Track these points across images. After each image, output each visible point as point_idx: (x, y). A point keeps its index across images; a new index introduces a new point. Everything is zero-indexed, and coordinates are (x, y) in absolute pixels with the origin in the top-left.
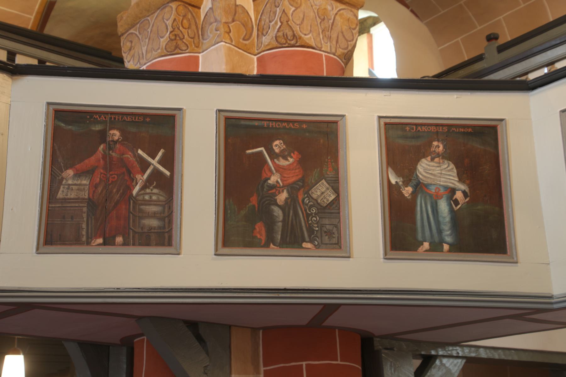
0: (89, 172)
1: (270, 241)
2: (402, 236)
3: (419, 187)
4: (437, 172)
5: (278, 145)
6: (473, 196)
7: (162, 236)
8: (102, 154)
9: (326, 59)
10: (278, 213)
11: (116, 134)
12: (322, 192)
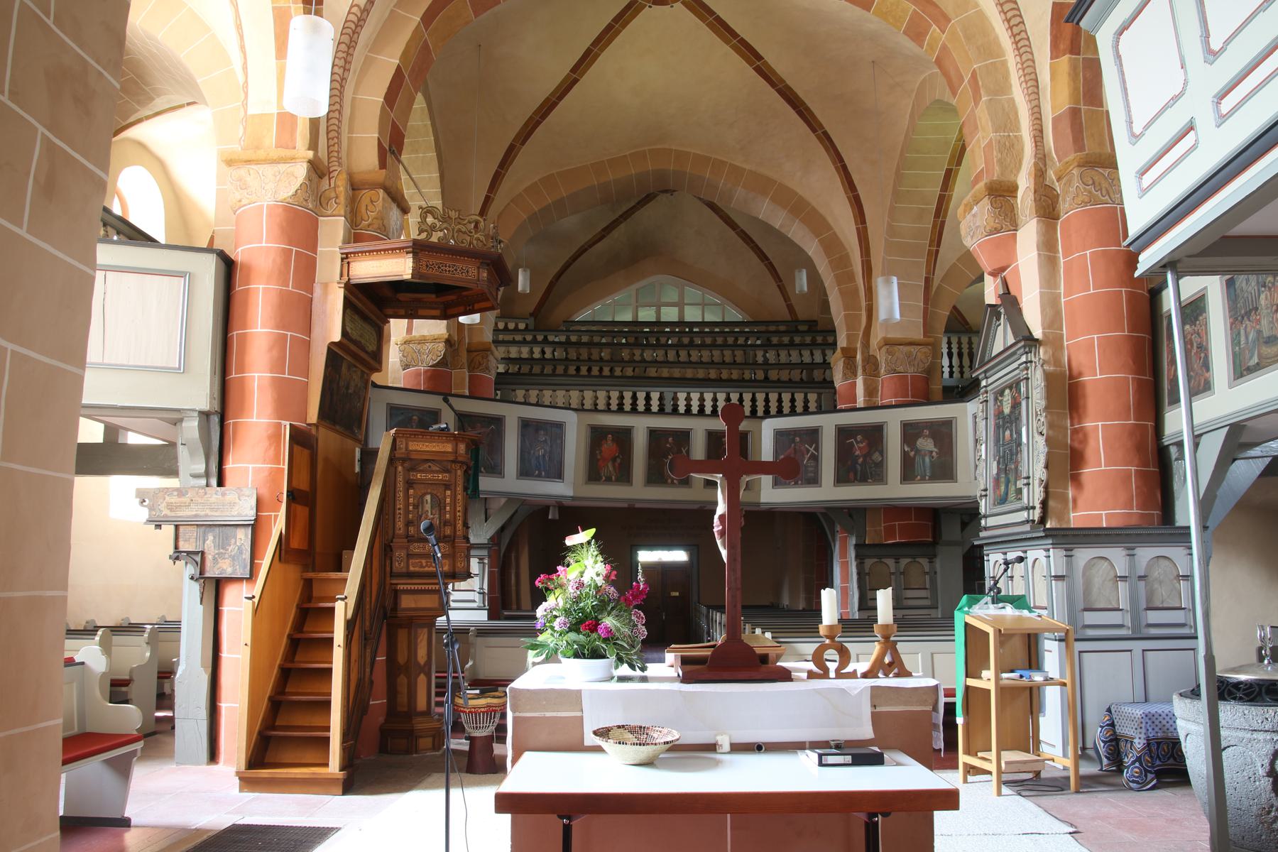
1: (856, 479)
3: (918, 451)
4: (926, 444)
5: (859, 438)
10: (859, 468)
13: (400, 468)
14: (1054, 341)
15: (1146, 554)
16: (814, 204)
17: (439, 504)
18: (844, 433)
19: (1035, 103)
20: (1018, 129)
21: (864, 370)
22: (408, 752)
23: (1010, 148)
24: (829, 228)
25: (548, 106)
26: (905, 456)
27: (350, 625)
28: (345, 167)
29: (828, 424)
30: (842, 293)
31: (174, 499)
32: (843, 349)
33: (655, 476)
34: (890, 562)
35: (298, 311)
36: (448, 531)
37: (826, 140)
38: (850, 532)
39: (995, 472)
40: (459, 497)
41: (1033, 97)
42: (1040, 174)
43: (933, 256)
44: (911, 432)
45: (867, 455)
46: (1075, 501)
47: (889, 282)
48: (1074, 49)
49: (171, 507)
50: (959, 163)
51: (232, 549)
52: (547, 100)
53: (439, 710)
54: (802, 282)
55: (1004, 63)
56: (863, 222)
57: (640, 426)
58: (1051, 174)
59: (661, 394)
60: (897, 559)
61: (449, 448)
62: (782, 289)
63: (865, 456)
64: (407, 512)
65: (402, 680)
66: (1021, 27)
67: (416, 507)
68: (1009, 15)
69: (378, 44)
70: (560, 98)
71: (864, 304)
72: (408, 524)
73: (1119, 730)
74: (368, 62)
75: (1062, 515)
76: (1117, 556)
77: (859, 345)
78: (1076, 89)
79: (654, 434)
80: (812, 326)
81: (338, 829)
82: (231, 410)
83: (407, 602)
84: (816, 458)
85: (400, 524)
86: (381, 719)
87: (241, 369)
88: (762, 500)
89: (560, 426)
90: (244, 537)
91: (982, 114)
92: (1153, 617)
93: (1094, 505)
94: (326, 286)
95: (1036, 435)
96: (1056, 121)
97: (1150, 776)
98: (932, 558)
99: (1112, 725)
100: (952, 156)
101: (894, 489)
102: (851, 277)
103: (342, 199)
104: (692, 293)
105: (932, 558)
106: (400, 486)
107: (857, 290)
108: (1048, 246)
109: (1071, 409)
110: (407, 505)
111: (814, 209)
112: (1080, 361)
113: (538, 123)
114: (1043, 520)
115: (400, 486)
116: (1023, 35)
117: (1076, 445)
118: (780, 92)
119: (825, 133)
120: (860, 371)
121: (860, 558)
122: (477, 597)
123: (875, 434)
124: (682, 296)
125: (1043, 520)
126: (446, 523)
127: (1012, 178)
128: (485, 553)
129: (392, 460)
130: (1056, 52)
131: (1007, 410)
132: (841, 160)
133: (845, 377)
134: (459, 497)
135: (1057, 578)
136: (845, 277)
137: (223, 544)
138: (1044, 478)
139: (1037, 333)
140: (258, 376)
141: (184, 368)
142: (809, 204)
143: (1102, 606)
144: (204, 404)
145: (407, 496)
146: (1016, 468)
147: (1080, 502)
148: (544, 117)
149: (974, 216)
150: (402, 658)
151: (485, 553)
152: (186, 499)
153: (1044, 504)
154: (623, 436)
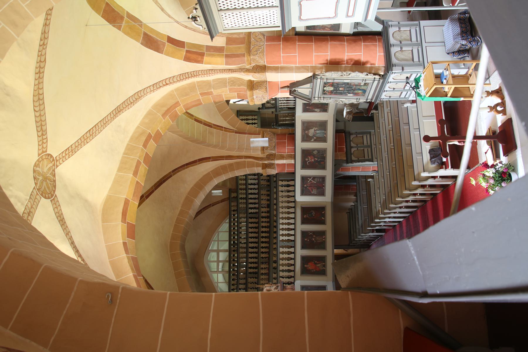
0: (312, 190)
1: (324, 161)
2: (324, 140)
3: (314, 135)
4: (311, 132)
5: (307, 160)
6: (316, 127)
7: (323, 179)
8: (320, 130)
9: (394, 9)
11: (305, 186)
12: (315, 152)
14: (313, 69)
15: (392, 41)
16: (197, 180)
18: (304, 166)
19: (218, 71)
20: (226, 79)
21: (273, 160)
23: (233, 82)
24: (208, 174)
26: (315, 141)
29: (300, 173)
30: (238, 169)
32: (262, 169)
33: (322, 246)
34: (353, 150)
37: (175, 171)
39: (352, 95)
41: (216, 72)
42: (248, 71)
43: (226, 129)
44: (306, 138)
45: (314, 156)
46: (371, 64)
47: (253, 142)
48: (202, 55)
50: (192, 115)
54: (218, 192)
55: (198, 82)
56: (209, 158)
58: (248, 67)
59: (281, 247)
60: (351, 147)
62: (218, 203)
63: (315, 157)
66: (189, 73)
68: (184, 77)
71: (243, 160)
73: (456, 50)
75: (378, 69)
76: (393, 50)
77: (261, 162)
78: (218, 55)
79: (303, 247)
80: (230, 191)
84: (314, 178)
88: (330, 201)
91: (215, 92)
92: (414, 39)
93: (374, 56)
95: (350, 76)
96: (227, 64)
97: (476, 39)
98: (350, 134)
99: (453, 52)
100: (190, 118)
101: (329, 145)
102: (231, 165)
104: (213, 246)
105: (350, 134)
107: (236, 163)
108: (276, 69)
109: (338, 64)
112: (322, 60)
114: (380, 75)
116: (192, 73)
117: (352, 63)
118: (156, 189)
120: (272, 162)
121: (352, 162)
123: (306, 153)
125: (380, 75)
127: (246, 82)
130: (200, 62)
131: (332, 89)
132: (184, 166)
133: (274, 168)
135: (403, 69)
136: (231, 168)
138: (366, 73)
139: (311, 74)
143: (411, 56)
146: (356, 85)
147: (372, 62)
149: (257, 97)
153: (374, 74)
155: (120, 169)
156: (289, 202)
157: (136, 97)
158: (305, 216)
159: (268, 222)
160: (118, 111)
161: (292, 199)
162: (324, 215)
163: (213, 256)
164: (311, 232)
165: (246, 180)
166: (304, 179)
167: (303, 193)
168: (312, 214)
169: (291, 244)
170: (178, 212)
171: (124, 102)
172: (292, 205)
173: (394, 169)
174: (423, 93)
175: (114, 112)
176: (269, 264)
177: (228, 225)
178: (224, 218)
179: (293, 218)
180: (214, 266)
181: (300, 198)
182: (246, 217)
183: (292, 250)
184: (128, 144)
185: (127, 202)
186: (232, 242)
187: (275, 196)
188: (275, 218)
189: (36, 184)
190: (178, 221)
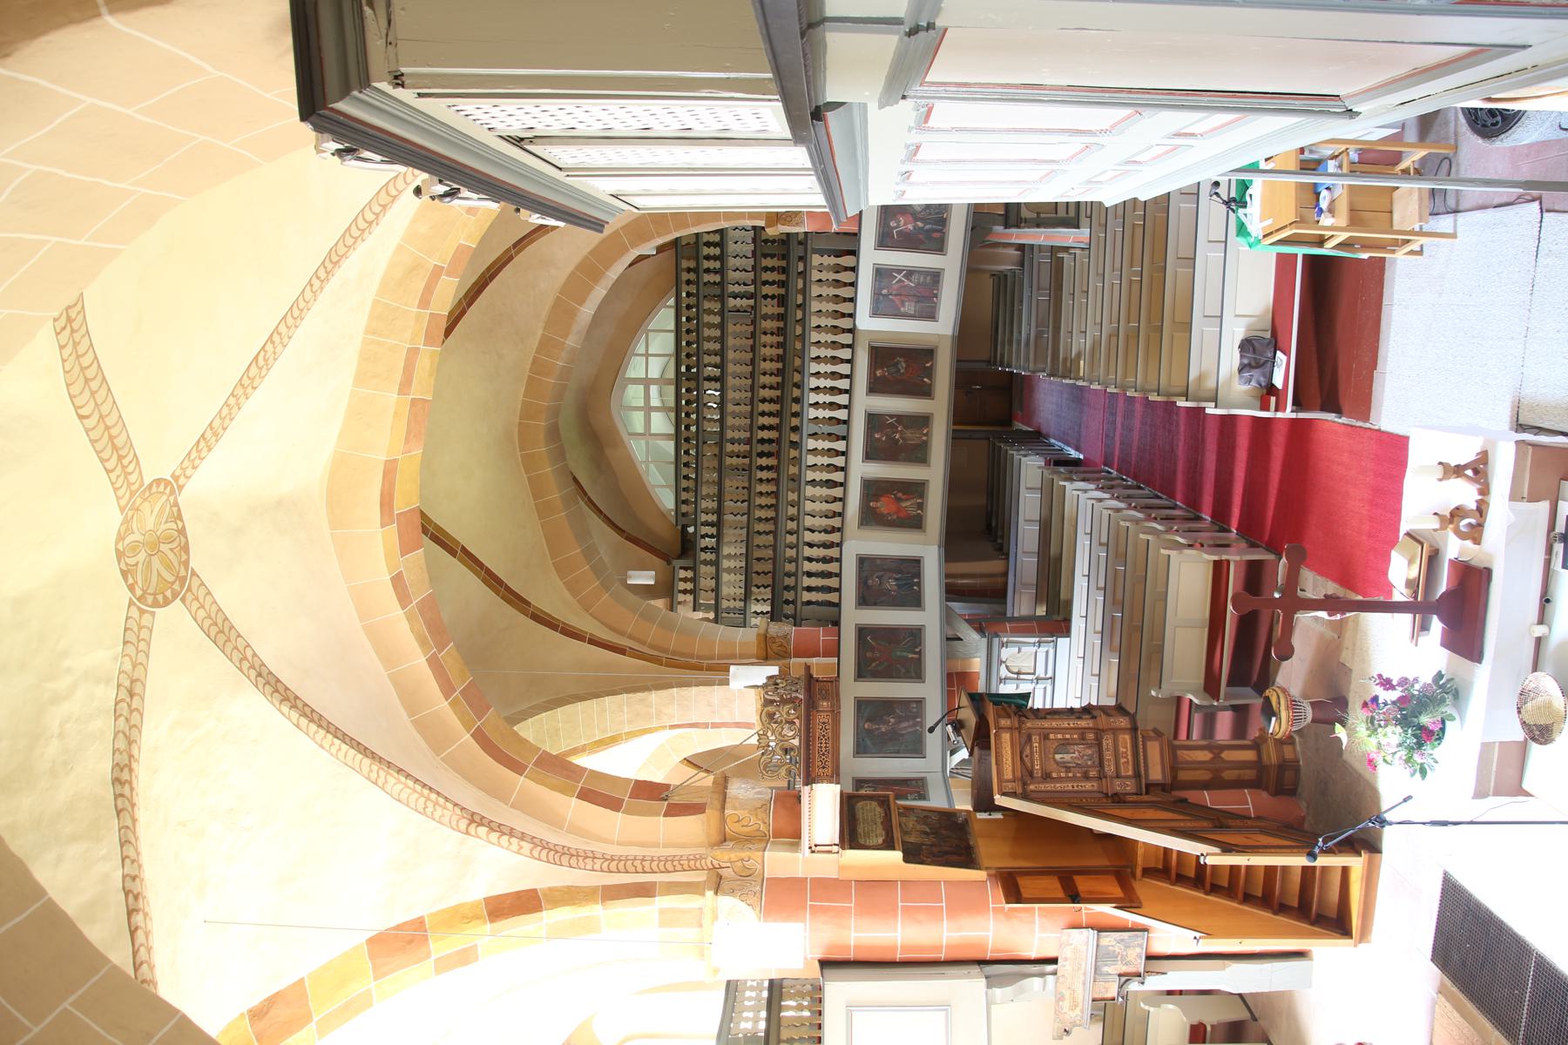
0: (903, 303)
5: (893, 224)
13: (1032, 787)
17: (1064, 745)
22: (1297, 770)
25: (491, 580)
27: (1227, 849)
28: (702, 851)
31: (1066, 1005)
33: (918, 454)
35: (872, 890)
36: (1091, 736)
38: (990, 231)
40: (1054, 724)
49: (1074, 1006)
51: (1118, 948)
52: (484, 581)
53: (889, 544)
57: (861, 469)
61: (1006, 737)
63: (916, 219)
64: (1074, 779)
65: (1228, 775)
67: (1068, 769)
69: (555, 822)
70: (481, 565)
72: (1086, 777)
74: (575, 830)
79: (870, 455)
81: (1445, 873)
82: (979, 956)
83: (1156, 774)
84: (910, 273)
85: (1088, 786)
86: (1265, 795)
87: (939, 948)
89: (862, 561)
90: (1109, 939)
94: (841, 868)
101: (938, 406)
103: (744, 855)
104: (636, 368)
106: (1049, 786)
110: (1067, 779)
111: (591, 253)
113: (508, 589)
115: (1049, 786)
118: (469, 305)
119: (515, 246)
122: (1043, 649)
124: (636, 381)
126: (1083, 738)
128: (996, 641)
129: (1025, 796)
134: (1054, 724)
137: (1113, 957)
140: (945, 934)
141: (944, 1006)
142: (586, 258)
144: (981, 983)
145: (1059, 779)
148: (500, 582)
150: (1204, 776)
151: (996, 641)
152: (1067, 993)
154: (873, 489)
155: (360, 379)
156: (835, 329)
157: (384, 199)
158: (879, 373)
159: (779, 345)
160: (332, 261)
161: (845, 323)
162: (930, 372)
163: (634, 394)
164: (891, 416)
165: (720, 244)
166: (881, 273)
167: (876, 312)
168: (899, 367)
169: (840, 430)
170: (534, 343)
171: (349, 229)
172: (846, 339)
173: (1136, 287)
174: (1256, 227)
175: (322, 271)
176: (776, 524)
177: (672, 312)
178: (662, 295)
179: (845, 407)
180: (637, 421)
181: (866, 321)
182: (721, 313)
183: (840, 446)
184: (376, 303)
185: (390, 470)
186: (683, 369)
187: (800, 301)
188: (798, 346)
189: (131, 588)
190: (538, 367)
